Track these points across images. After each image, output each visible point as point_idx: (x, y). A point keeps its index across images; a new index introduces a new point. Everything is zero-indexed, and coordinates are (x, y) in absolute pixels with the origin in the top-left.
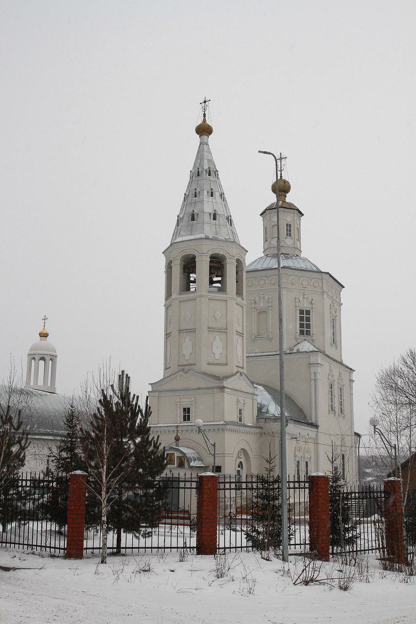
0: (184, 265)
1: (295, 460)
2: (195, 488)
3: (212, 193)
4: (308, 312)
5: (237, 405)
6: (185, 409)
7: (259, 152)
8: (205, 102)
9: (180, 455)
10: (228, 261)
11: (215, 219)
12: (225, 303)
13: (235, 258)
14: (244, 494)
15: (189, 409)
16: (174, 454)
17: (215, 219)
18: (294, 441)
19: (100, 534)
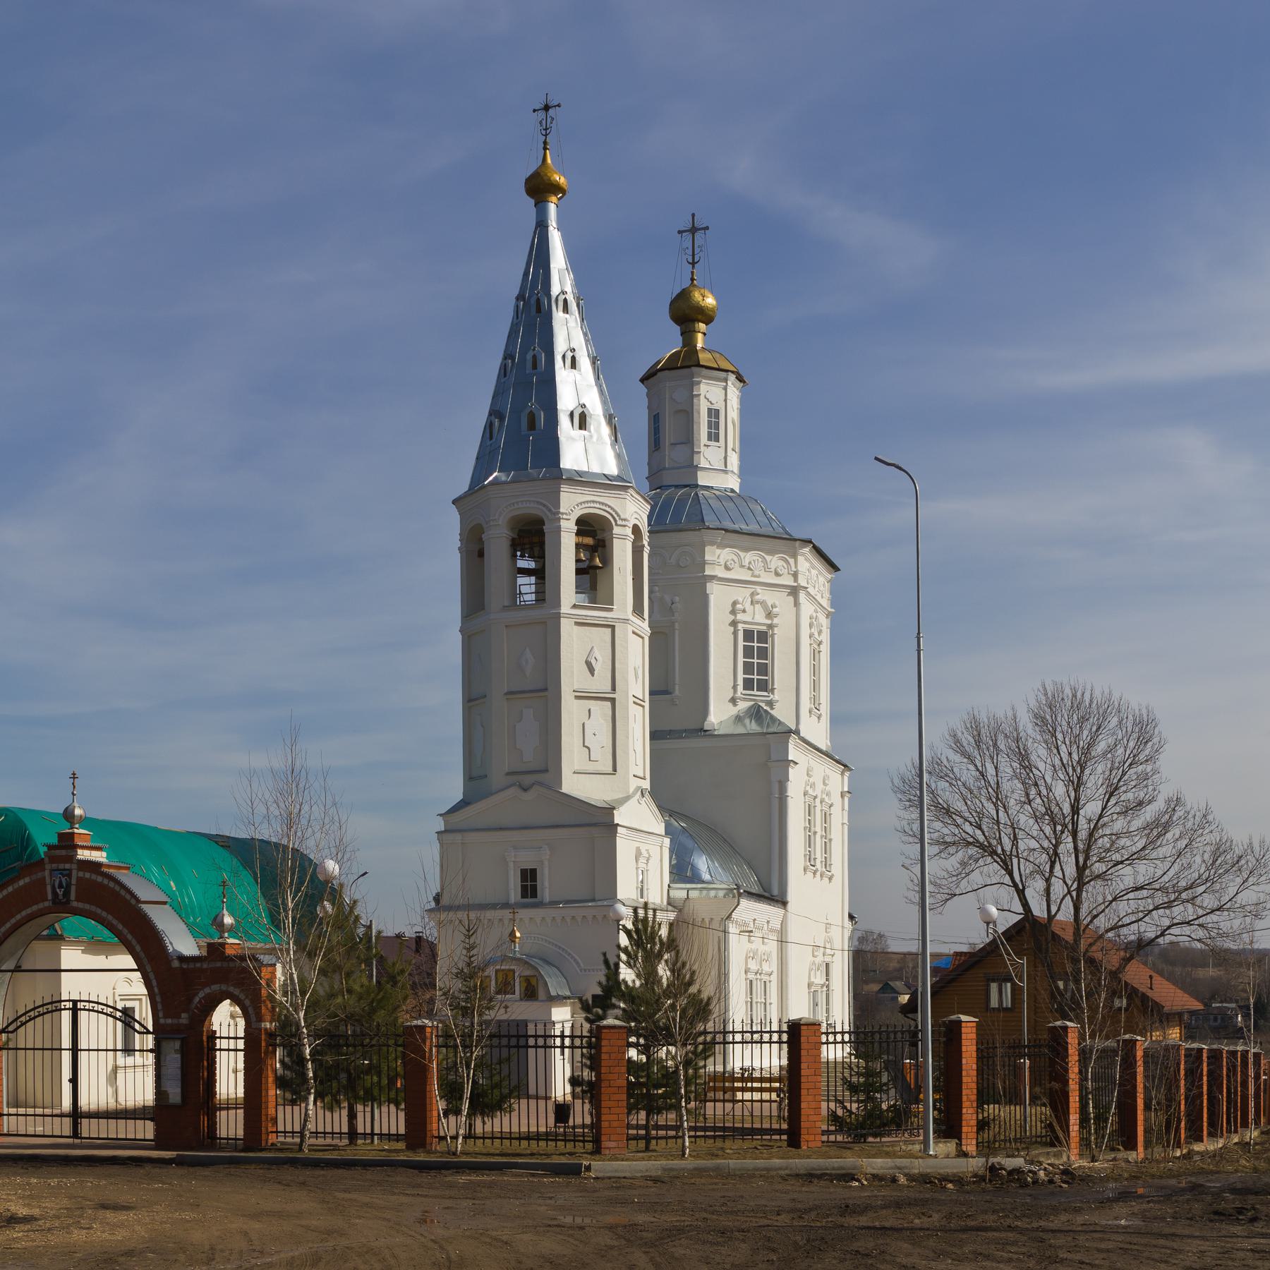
0: (513, 540)
3: (573, 358)
4: (763, 637)
6: (524, 873)
7: (877, 459)
8: (547, 108)
9: (528, 973)
10: (616, 530)
15: (533, 871)
16: (513, 971)
18: (744, 938)
19: (1161, 1149)
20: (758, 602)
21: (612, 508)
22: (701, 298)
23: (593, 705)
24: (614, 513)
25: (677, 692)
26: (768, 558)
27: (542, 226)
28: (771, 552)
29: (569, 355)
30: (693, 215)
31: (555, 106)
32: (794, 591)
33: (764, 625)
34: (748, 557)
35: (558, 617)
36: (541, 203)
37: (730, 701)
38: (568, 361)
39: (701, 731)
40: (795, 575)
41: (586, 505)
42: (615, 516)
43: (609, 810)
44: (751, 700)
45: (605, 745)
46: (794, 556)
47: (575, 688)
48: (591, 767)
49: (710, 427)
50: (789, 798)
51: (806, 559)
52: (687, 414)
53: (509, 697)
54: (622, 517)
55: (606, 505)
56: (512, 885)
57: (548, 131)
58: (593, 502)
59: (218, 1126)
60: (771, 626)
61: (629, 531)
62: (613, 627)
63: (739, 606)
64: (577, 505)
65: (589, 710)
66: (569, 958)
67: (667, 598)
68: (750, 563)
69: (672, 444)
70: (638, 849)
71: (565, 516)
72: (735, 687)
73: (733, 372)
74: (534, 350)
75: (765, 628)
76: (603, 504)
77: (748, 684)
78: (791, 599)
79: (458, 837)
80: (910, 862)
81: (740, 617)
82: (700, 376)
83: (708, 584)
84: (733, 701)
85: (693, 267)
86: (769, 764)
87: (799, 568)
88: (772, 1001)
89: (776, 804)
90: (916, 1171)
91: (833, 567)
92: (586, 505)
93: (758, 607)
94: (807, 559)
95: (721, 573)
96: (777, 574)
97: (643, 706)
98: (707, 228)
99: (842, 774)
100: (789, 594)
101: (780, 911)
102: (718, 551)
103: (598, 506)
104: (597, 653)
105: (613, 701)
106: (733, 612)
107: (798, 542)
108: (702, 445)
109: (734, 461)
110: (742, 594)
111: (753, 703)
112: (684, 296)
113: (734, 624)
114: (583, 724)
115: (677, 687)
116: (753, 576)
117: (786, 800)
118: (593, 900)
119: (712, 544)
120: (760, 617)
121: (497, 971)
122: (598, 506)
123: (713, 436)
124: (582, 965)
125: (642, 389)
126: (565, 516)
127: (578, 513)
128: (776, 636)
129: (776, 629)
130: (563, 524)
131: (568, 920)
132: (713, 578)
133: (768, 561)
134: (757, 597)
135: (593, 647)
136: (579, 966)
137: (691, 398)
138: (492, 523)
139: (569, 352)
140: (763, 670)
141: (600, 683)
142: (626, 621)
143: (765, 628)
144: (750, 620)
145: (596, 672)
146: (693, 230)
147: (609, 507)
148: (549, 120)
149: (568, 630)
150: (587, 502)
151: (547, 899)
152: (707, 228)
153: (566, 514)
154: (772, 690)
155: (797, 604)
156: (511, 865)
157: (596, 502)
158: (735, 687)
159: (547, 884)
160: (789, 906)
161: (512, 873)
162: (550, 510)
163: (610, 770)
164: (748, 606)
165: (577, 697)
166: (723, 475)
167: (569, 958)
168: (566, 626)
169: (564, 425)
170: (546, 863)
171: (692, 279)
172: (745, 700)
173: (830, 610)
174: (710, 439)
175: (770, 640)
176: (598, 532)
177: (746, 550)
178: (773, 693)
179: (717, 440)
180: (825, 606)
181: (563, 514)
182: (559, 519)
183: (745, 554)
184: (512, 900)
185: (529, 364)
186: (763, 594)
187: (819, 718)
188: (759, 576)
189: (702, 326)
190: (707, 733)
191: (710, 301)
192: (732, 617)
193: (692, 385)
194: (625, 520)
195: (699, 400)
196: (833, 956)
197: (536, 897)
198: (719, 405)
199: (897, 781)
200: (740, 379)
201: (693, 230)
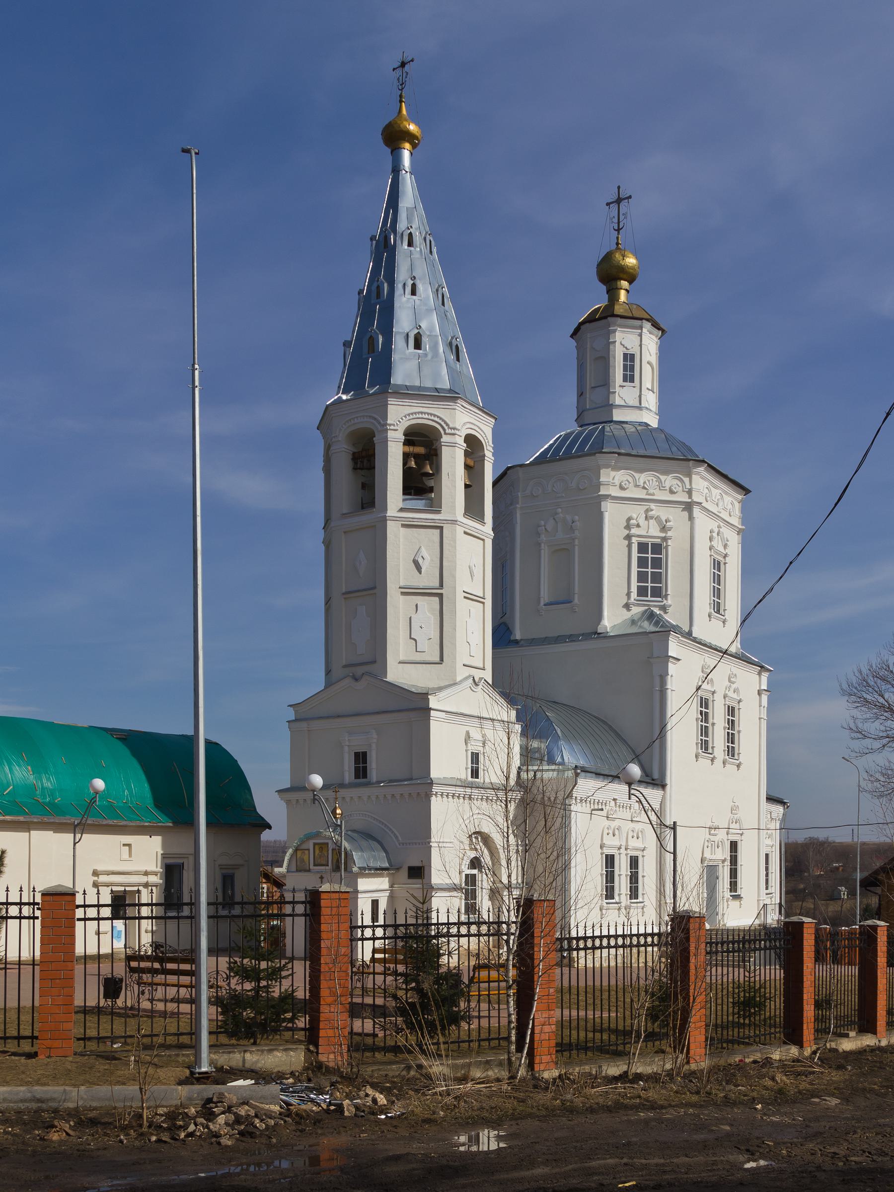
0: (354, 454)
1: (602, 854)
2: (302, 903)
3: (414, 287)
4: (657, 548)
5: (466, 744)
6: (357, 755)
8: (403, 65)
10: (445, 438)
11: (418, 345)
12: (437, 531)
13: (463, 433)
14: (411, 916)
15: (364, 754)
17: (418, 345)
20: (652, 518)
21: (441, 418)
22: (621, 258)
23: (422, 601)
24: (443, 423)
25: (576, 601)
26: (663, 478)
27: (396, 170)
28: (666, 473)
29: (410, 282)
30: (619, 188)
31: (409, 62)
32: (688, 507)
33: (658, 537)
34: (642, 478)
35: (384, 520)
36: (396, 151)
37: (624, 607)
38: (408, 289)
39: (597, 635)
40: (690, 492)
41: (414, 416)
42: (444, 425)
43: (424, 696)
44: (645, 605)
45: (432, 637)
46: (689, 476)
47: (402, 584)
48: (418, 657)
49: (625, 369)
50: (669, 692)
51: (702, 478)
52: (604, 360)
53: (345, 596)
54: (451, 425)
55: (435, 416)
56: (346, 768)
57: (403, 86)
58: (422, 413)
59: (308, 979)
60: (665, 539)
61: (461, 440)
62: (441, 528)
63: (633, 522)
64: (405, 417)
65: (417, 606)
66: (390, 833)
67: (569, 518)
68: (645, 483)
69: (592, 388)
70: (468, 733)
71: (392, 427)
72: (629, 594)
73: (648, 320)
74: (378, 281)
75: (659, 540)
76: (431, 414)
77: (642, 591)
78: (686, 514)
79: (304, 725)
80: (854, 754)
81: (634, 531)
82: (615, 325)
83: (602, 503)
84: (627, 606)
85: (618, 233)
86: (651, 660)
87: (694, 486)
88: (622, 873)
89: (657, 696)
90: (71, 1105)
91: (746, 491)
92: (414, 416)
93: (652, 522)
94: (703, 478)
95: (615, 492)
96: (672, 492)
97: (483, 603)
98: (630, 197)
99: (759, 674)
100: (684, 510)
101: (661, 792)
102: (613, 473)
103: (426, 416)
104: (424, 552)
105: (440, 596)
106: (628, 527)
107: (691, 462)
108: (617, 385)
109: (651, 400)
110: (637, 512)
111: (647, 608)
112: (608, 257)
113: (628, 537)
114: (410, 618)
115: (576, 596)
116: (648, 494)
117: (666, 693)
118: (411, 779)
119: (607, 466)
120: (654, 531)
121: (315, 844)
122: (426, 416)
123: (629, 377)
124: (400, 839)
125: (573, 343)
126: (392, 427)
127: (406, 424)
128: (670, 548)
129: (669, 541)
130: (391, 434)
131: (389, 797)
132: (607, 497)
133: (663, 481)
134: (650, 513)
135: (420, 547)
136: (398, 840)
137: (608, 345)
138: (334, 440)
139: (410, 280)
140: (657, 578)
141: (429, 579)
142: (454, 522)
143: (659, 540)
144: (643, 533)
145: (423, 570)
146: (619, 201)
147: (438, 417)
148: (404, 74)
149: (394, 531)
150: (415, 413)
151: (374, 780)
152: (630, 197)
153: (394, 425)
154: (666, 596)
155: (691, 518)
156: (346, 748)
157: (425, 413)
158: (629, 594)
159: (374, 765)
160: (668, 787)
161: (346, 756)
162: (379, 423)
163: (437, 659)
164: (642, 521)
165: (403, 594)
166: (638, 412)
167: (390, 833)
168: (393, 528)
169: (398, 343)
170: (374, 746)
171: (617, 244)
172: (638, 605)
173: (740, 527)
174: (625, 380)
175: (664, 551)
176: (434, 442)
177: (641, 471)
178: (666, 599)
179: (632, 380)
180: (736, 524)
181: (390, 425)
182: (387, 430)
183: (640, 475)
184: (347, 781)
185: (374, 295)
186: (657, 510)
187: (724, 622)
188: (653, 495)
189: (625, 284)
190: (601, 635)
191: (631, 261)
192: (627, 532)
193: (608, 333)
194: (454, 429)
195: (615, 346)
196: (741, 835)
197: (367, 778)
198: (635, 351)
199: (845, 686)
200: (656, 325)
201: (619, 201)
